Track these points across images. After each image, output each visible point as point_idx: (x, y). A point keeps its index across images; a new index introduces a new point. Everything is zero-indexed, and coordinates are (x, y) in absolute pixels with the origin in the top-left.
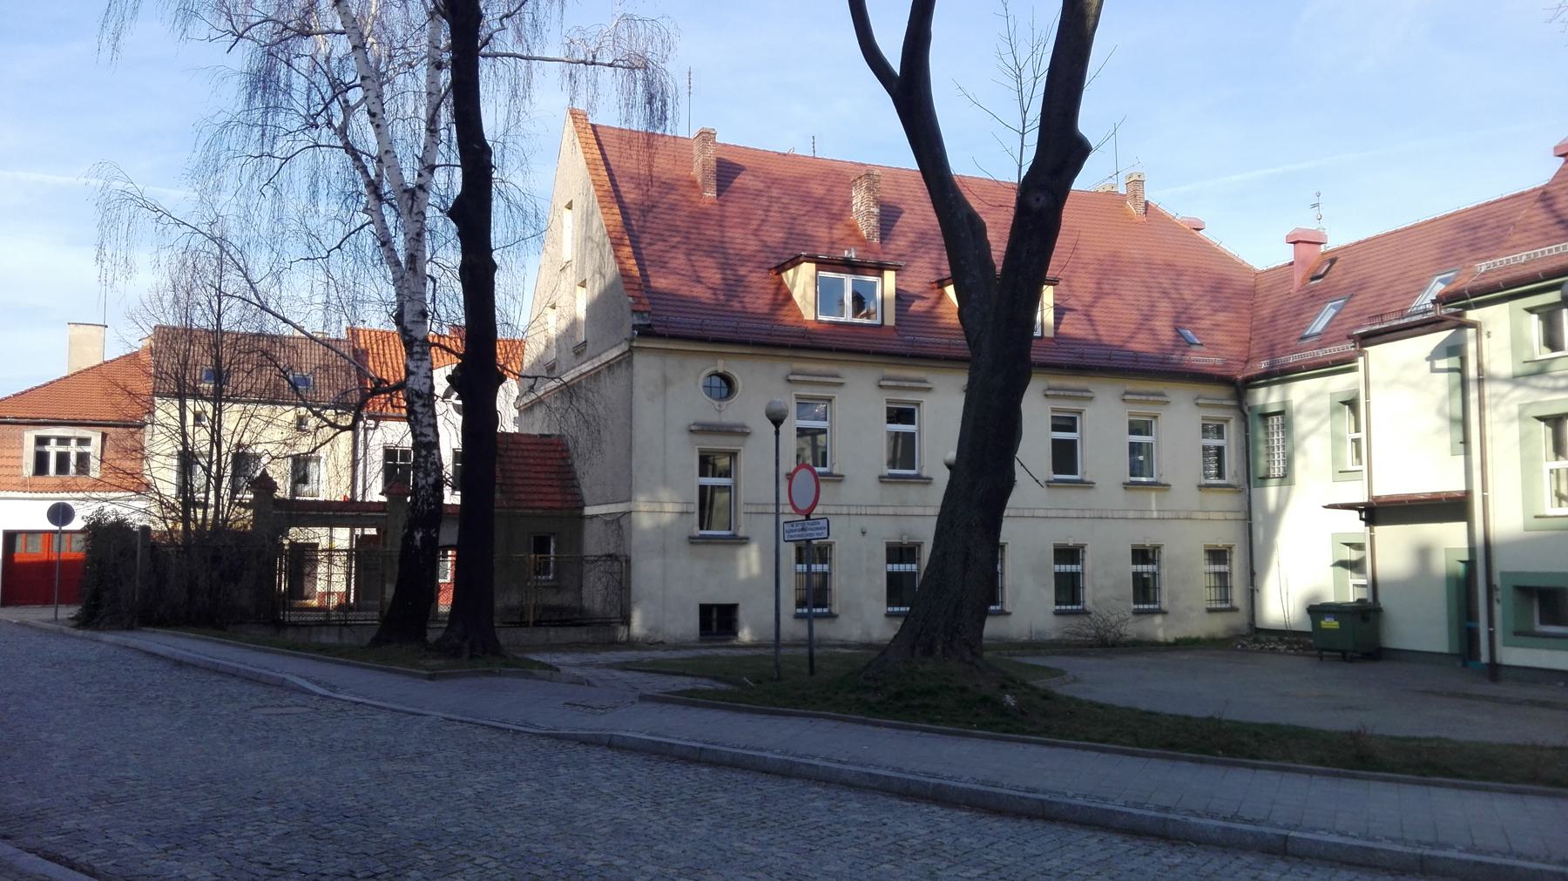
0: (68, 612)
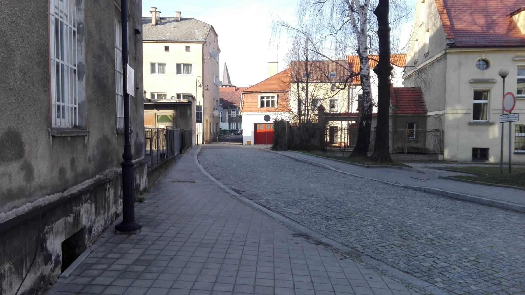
0: (270, 146)
